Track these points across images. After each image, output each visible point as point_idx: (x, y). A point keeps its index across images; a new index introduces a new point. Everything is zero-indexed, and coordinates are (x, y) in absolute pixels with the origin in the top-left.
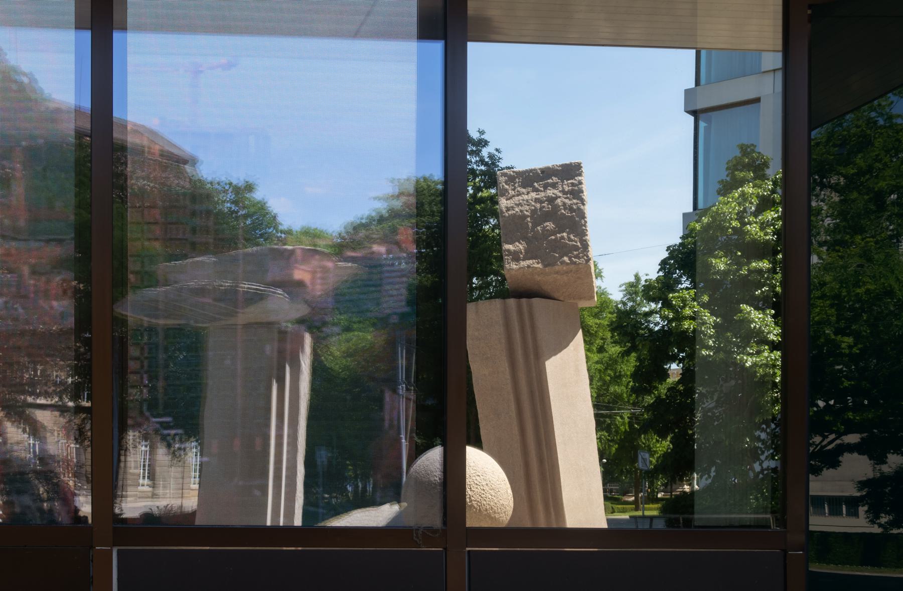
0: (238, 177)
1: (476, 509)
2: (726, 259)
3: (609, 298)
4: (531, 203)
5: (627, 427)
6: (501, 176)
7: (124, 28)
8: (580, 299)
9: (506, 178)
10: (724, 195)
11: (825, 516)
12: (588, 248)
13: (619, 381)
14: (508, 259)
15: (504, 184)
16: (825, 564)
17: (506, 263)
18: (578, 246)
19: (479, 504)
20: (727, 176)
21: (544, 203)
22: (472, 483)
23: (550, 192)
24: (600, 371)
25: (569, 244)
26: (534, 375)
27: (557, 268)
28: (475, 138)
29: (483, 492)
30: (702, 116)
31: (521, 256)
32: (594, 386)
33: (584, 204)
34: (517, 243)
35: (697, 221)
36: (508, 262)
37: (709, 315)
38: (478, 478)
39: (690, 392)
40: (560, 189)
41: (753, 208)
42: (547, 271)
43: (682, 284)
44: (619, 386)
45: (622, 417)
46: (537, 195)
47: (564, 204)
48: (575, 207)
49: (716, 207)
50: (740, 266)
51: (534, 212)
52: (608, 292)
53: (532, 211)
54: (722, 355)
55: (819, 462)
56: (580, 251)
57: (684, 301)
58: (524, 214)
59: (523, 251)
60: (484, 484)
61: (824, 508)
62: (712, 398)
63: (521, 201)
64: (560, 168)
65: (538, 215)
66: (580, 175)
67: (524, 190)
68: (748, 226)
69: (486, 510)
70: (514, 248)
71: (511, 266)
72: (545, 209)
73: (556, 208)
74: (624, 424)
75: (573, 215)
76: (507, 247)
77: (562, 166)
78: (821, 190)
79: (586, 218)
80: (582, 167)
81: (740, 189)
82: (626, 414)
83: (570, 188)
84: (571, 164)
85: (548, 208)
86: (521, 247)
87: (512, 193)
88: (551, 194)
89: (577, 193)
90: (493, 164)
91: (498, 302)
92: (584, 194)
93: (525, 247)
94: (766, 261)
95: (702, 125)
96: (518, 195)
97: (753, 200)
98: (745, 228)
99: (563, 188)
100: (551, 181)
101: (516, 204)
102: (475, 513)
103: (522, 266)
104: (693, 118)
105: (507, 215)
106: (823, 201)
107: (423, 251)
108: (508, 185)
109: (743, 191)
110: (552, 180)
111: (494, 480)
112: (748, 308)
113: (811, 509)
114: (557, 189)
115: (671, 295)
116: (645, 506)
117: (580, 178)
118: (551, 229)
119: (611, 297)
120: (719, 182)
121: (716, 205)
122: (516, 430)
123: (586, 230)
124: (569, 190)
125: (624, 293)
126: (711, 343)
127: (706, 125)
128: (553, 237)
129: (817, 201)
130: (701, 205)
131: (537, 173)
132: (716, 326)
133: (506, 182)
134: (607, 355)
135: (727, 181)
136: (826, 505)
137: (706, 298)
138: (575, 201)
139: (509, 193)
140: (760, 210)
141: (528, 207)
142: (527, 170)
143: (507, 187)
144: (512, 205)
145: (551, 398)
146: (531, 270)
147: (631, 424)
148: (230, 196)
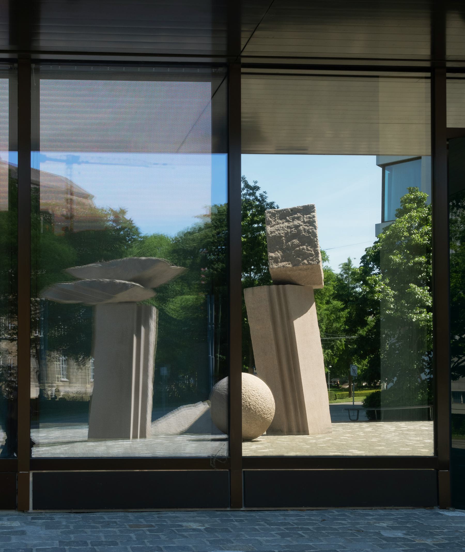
0: (116, 207)
1: (253, 411)
2: (400, 256)
3: (333, 273)
4: (285, 229)
5: (344, 347)
6: (268, 213)
7: (37, 149)
8: (314, 284)
9: (270, 214)
10: (399, 217)
11: (461, 404)
12: (318, 255)
13: (339, 320)
14: (271, 262)
15: (269, 218)
16: (461, 435)
17: (270, 264)
18: (313, 254)
19: (254, 407)
20: (401, 206)
21: (292, 228)
22: (250, 395)
23: (296, 222)
24: (327, 315)
25: (307, 253)
26: (287, 329)
27: (300, 267)
28: (252, 185)
29: (256, 400)
30: (387, 167)
31: (279, 260)
32: (324, 323)
33: (316, 229)
34: (277, 252)
35: (384, 233)
36: (271, 264)
37: (390, 290)
38: (253, 392)
39: (378, 334)
40: (302, 221)
41: (416, 225)
42: (295, 269)
43: (374, 270)
44: (338, 323)
45: (341, 341)
46: (288, 224)
47: (304, 229)
48: (310, 231)
49: (394, 224)
50: (409, 260)
51: (286, 234)
52: (332, 269)
53: (286, 233)
54: (399, 314)
55: (457, 373)
56: (314, 257)
57: (375, 281)
58: (281, 235)
59: (280, 257)
60: (257, 395)
61: (461, 399)
62: (394, 337)
63: (279, 228)
64: (302, 208)
65: (289, 235)
66: (314, 212)
67: (280, 221)
68: (414, 235)
69: (259, 412)
70: (275, 255)
71: (273, 266)
72: (293, 232)
73: (299, 231)
74: (341, 345)
75: (310, 235)
76: (271, 254)
77: (303, 207)
78: (457, 209)
79: (317, 237)
80: (315, 207)
81: (409, 214)
82: (343, 339)
83: (308, 220)
84: (308, 205)
85: (295, 231)
86: (279, 255)
87: (274, 223)
88: (297, 224)
89: (312, 223)
90: (263, 200)
91: (265, 288)
92: (316, 223)
93: (281, 255)
94: (424, 257)
95: (387, 172)
96: (277, 224)
97: (416, 220)
98: (411, 237)
99: (304, 220)
100: (297, 216)
101: (276, 230)
102: (252, 413)
103: (280, 266)
104: (382, 168)
105: (271, 236)
106: (458, 216)
107: (223, 247)
108: (272, 218)
109: (410, 215)
110: (297, 215)
111: (264, 393)
112: (414, 286)
113: (452, 399)
114: (300, 221)
115: (368, 278)
116: (355, 392)
117: (314, 214)
118: (297, 244)
119: (334, 272)
120: (396, 210)
121: (394, 223)
122: (276, 362)
123: (318, 244)
124: (307, 221)
125: (342, 269)
126: (392, 306)
127: (389, 172)
128: (298, 249)
129: (455, 216)
130: (386, 219)
131: (288, 211)
132: (394, 296)
133: (270, 217)
134: (332, 305)
135: (401, 209)
136: (462, 397)
137: (388, 281)
138: (311, 227)
139: (272, 223)
140: (420, 226)
141: (283, 231)
142: (282, 209)
143: (271, 219)
144: (274, 230)
145: (297, 342)
146: (285, 268)
147: (346, 346)
148: (112, 217)
